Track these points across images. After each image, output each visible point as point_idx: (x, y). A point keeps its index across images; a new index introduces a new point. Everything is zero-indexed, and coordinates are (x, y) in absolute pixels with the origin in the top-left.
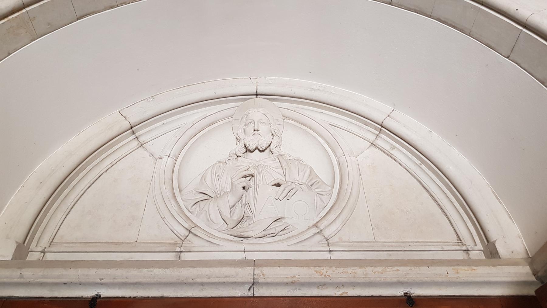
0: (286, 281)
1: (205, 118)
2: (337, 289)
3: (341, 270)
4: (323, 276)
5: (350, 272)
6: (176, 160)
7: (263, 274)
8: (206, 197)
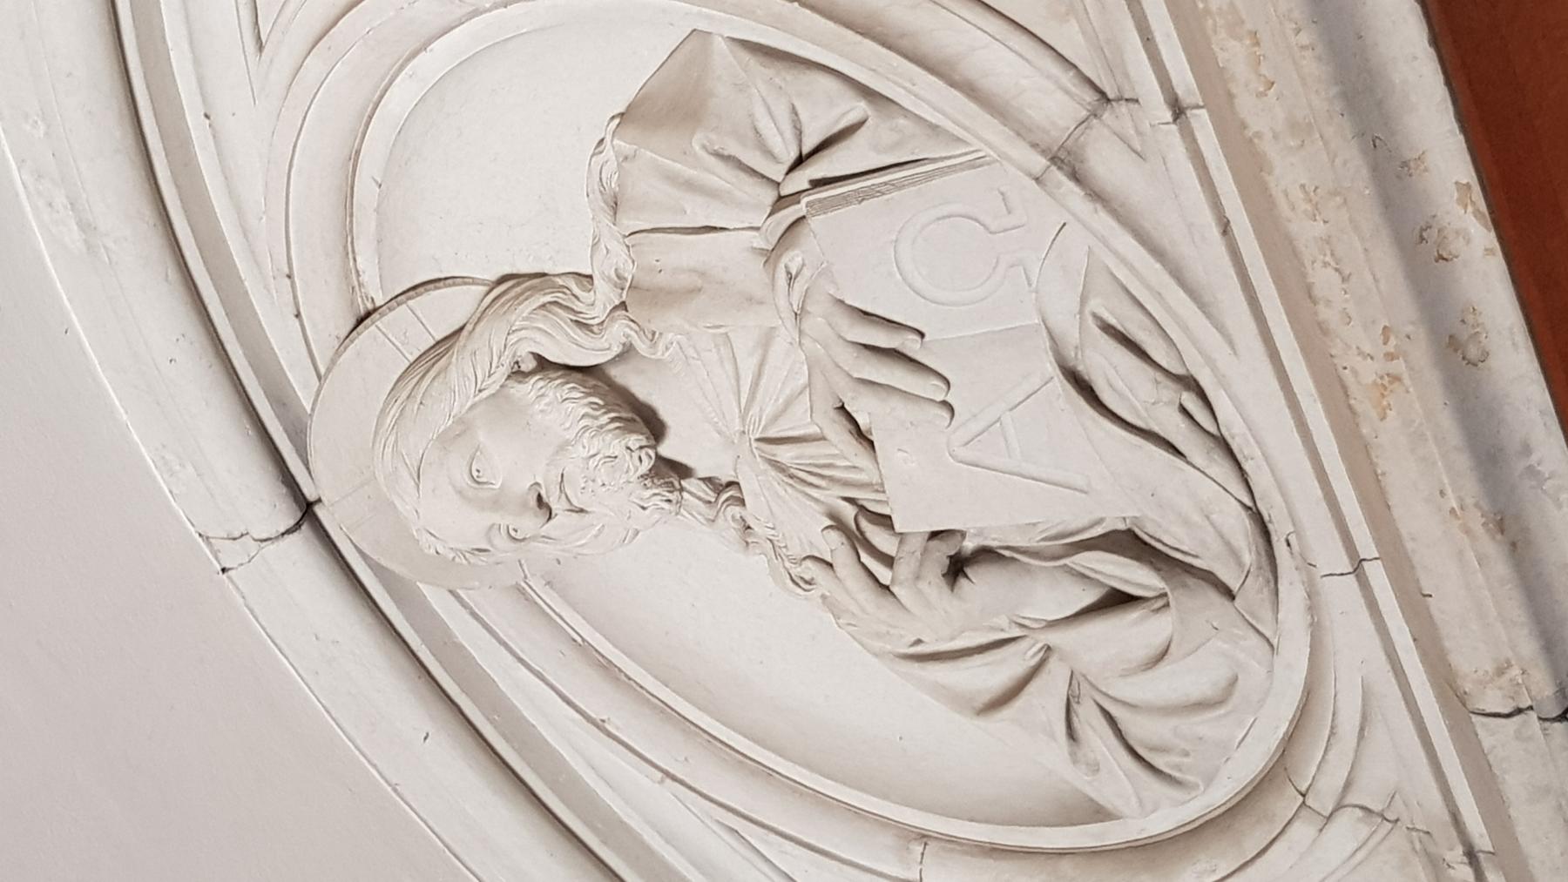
0: (1501, 567)
1: (599, 726)
2: (1456, 245)
3: (1324, 279)
4: (1399, 366)
5: (1319, 228)
6: (924, 837)
7: (1500, 672)
8: (1087, 717)
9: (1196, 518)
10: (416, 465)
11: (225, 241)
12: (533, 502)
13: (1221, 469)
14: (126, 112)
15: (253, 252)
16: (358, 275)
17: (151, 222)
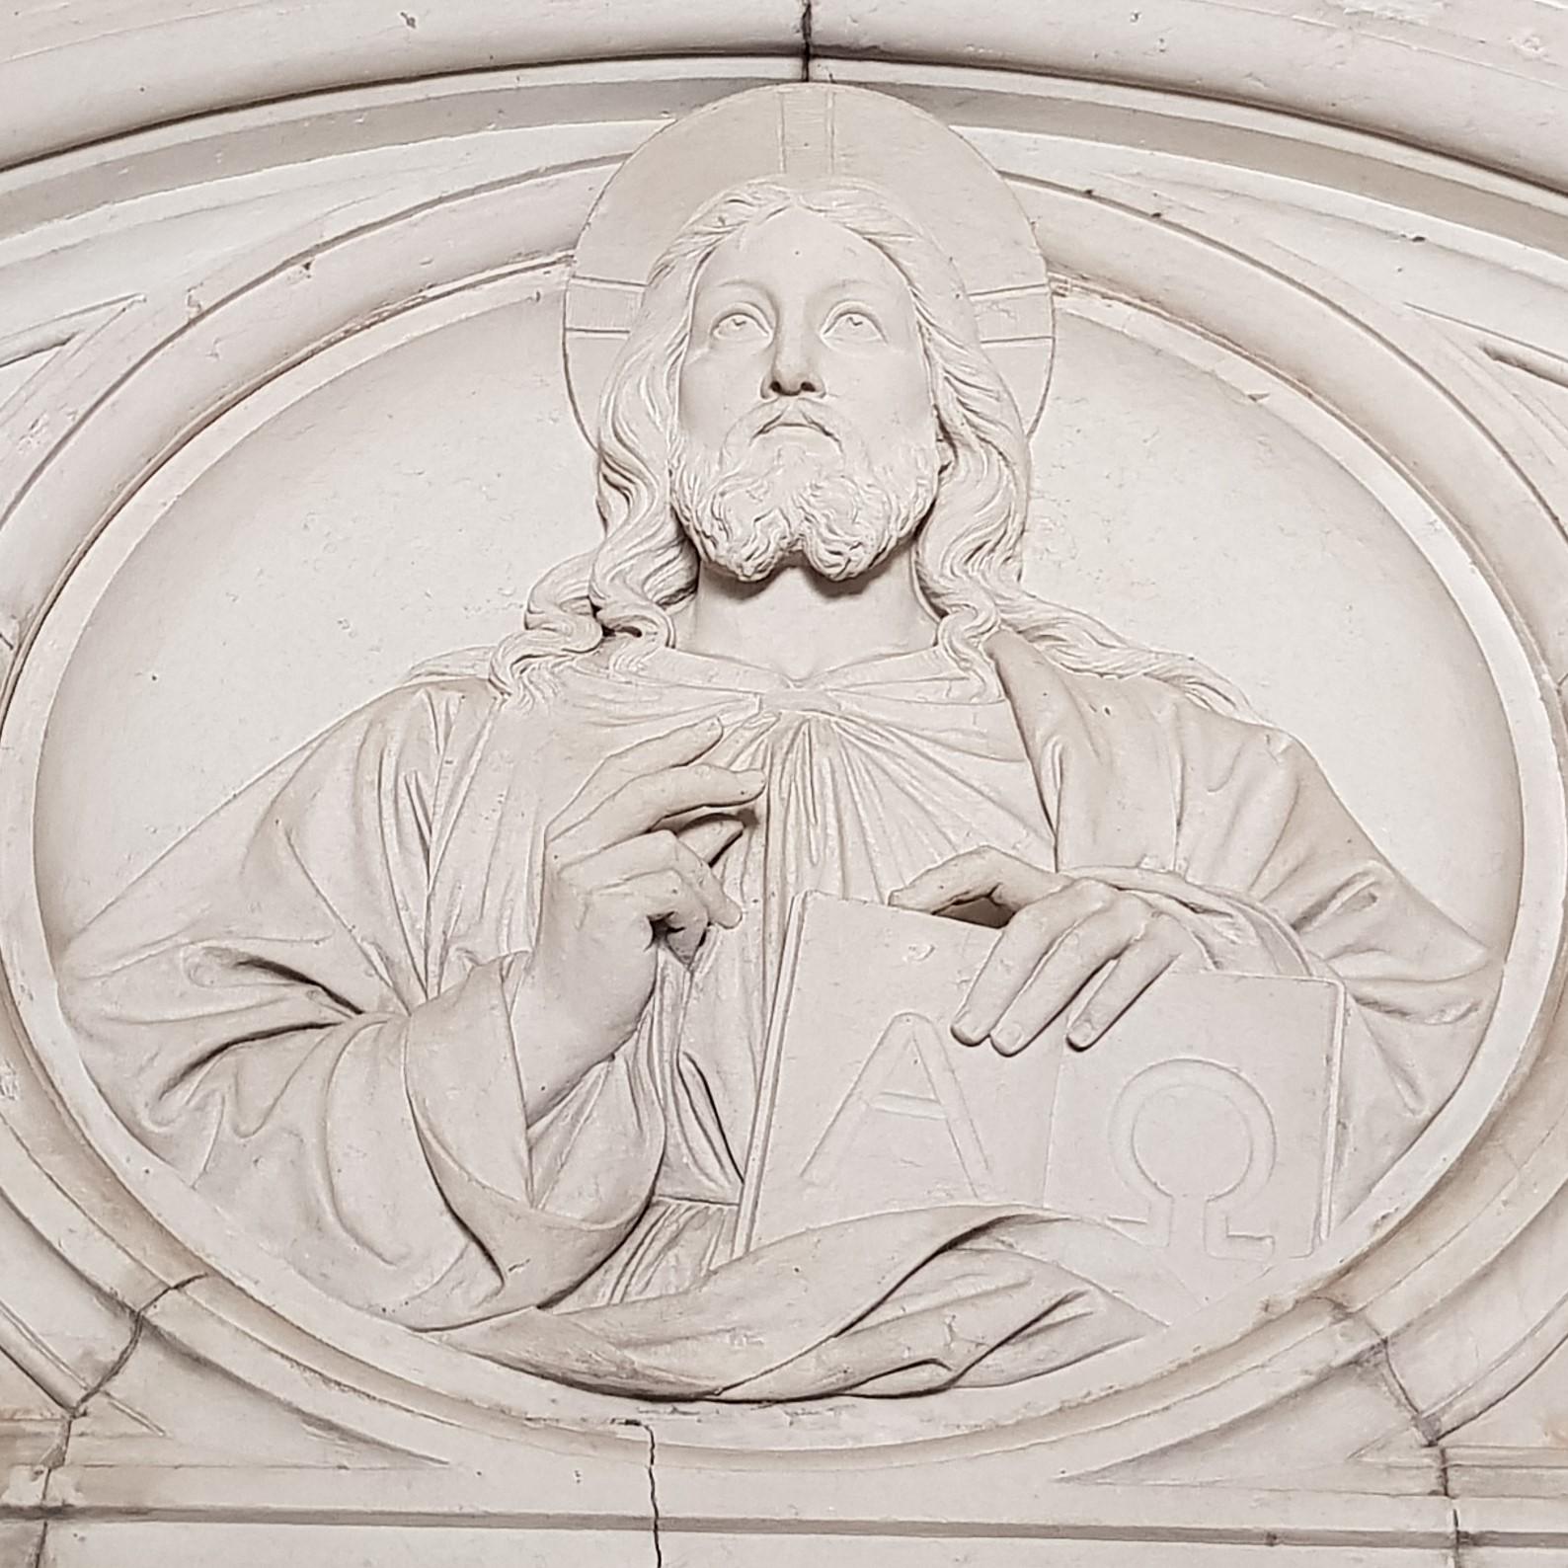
9: (737, 1316)
10: (892, 248)
11: (1223, 161)
12: (812, 379)
13: (810, 1375)
14: (1512, 161)
15: (1197, 187)
16: (1104, 296)
17: (1341, 104)
